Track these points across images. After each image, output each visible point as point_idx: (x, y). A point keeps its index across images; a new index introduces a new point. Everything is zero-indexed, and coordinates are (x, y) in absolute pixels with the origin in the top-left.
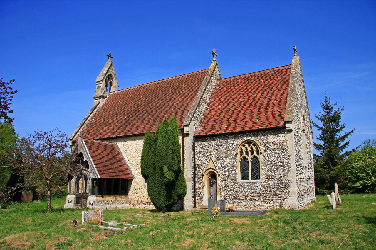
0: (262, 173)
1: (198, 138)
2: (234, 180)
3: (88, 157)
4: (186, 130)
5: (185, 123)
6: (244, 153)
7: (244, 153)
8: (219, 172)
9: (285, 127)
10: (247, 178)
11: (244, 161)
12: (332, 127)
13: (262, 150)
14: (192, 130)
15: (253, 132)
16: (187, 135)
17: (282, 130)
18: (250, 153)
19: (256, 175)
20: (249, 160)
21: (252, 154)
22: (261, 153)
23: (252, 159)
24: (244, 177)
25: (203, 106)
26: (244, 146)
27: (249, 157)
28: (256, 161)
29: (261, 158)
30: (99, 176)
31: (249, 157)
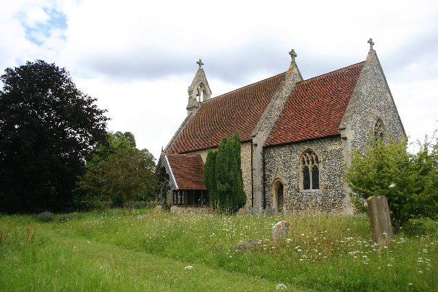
0: (321, 183)
1: (266, 148)
2: (298, 190)
3: (170, 170)
4: (254, 141)
5: (253, 133)
6: (306, 163)
7: (306, 163)
8: (284, 181)
9: (340, 135)
10: (309, 188)
11: (306, 170)
12: (60, 121)
13: (320, 159)
14: (261, 138)
15: (311, 141)
16: (256, 145)
17: (336, 137)
18: (311, 162)
19: (316, 186)
20: (310, 169)
21: (313, 163)
22: (320, 162)
23: (313, 168)
24: (306, 187)
25: (276, 114)
26: (306, 155)
27: (310, 167)
28: (316, 171)
29: (321, 168)
30: (177, 187)
31: (310, 167)
